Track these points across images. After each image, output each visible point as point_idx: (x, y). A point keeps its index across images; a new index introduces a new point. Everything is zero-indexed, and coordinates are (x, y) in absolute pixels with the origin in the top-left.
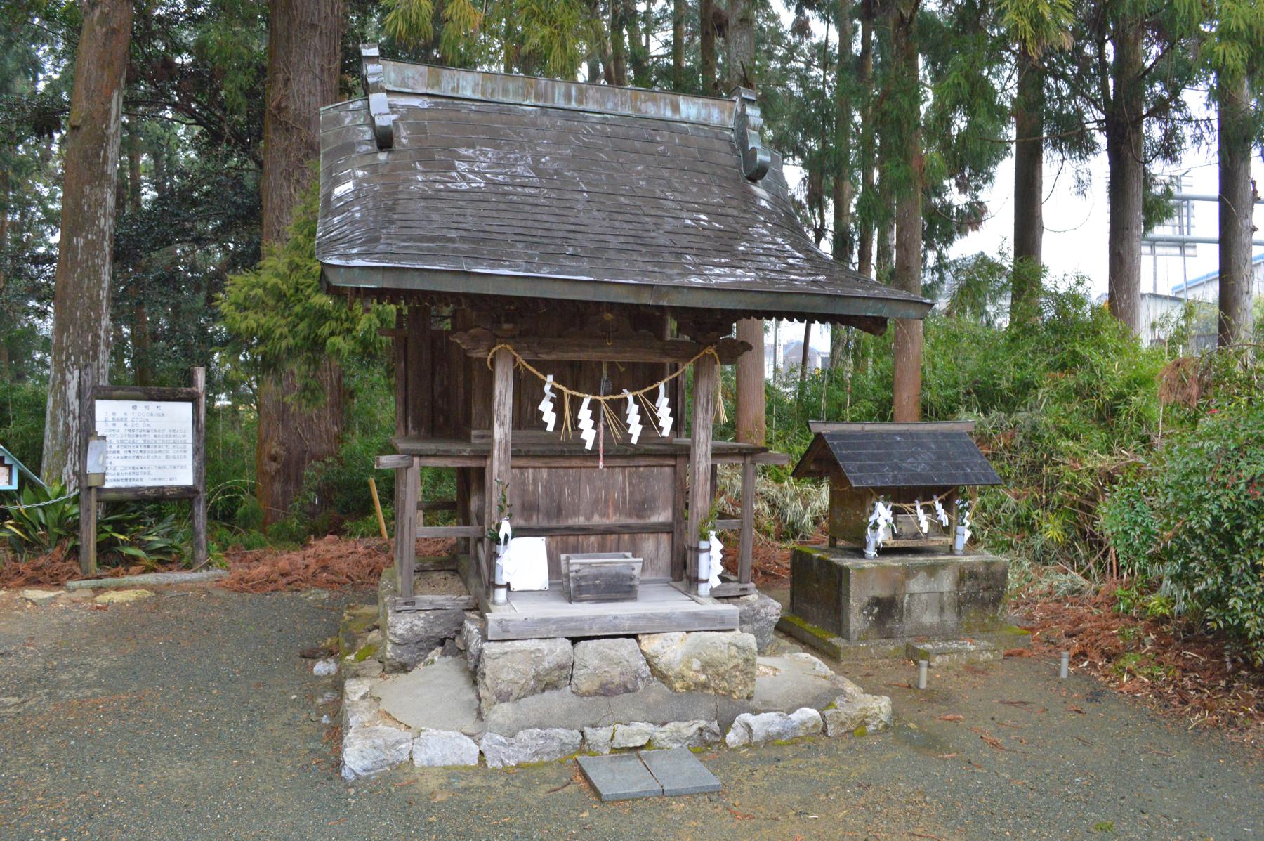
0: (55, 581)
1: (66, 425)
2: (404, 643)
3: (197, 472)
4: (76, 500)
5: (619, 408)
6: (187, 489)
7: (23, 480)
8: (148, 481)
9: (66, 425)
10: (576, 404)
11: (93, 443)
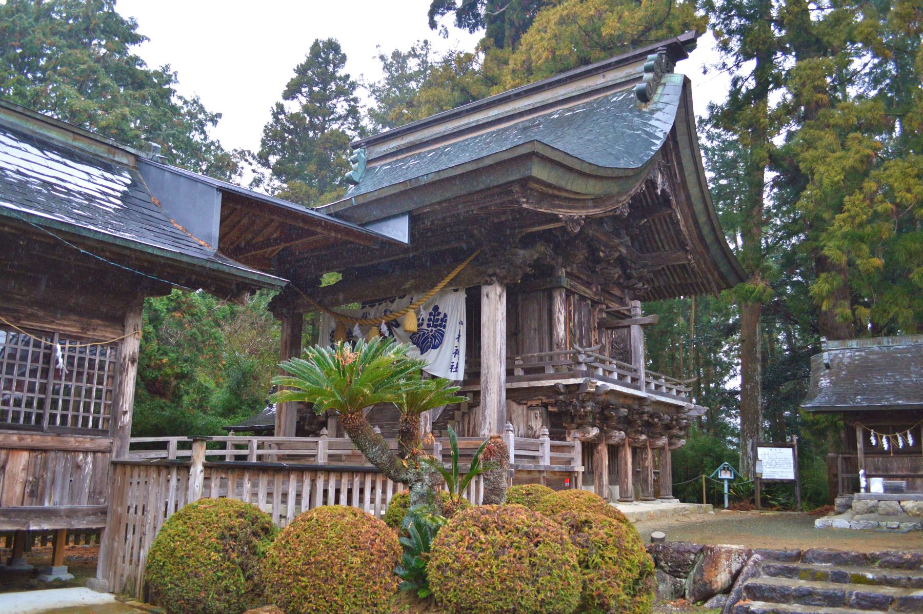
0: (747, 510)
2: (839, 506)
3: (795, 474)
4: (753, 483)
5: (896, 438)
6: (790, 482)
7: (735, 476)
8: (777, 477)
10: (882, 438)
11: (757, 462)
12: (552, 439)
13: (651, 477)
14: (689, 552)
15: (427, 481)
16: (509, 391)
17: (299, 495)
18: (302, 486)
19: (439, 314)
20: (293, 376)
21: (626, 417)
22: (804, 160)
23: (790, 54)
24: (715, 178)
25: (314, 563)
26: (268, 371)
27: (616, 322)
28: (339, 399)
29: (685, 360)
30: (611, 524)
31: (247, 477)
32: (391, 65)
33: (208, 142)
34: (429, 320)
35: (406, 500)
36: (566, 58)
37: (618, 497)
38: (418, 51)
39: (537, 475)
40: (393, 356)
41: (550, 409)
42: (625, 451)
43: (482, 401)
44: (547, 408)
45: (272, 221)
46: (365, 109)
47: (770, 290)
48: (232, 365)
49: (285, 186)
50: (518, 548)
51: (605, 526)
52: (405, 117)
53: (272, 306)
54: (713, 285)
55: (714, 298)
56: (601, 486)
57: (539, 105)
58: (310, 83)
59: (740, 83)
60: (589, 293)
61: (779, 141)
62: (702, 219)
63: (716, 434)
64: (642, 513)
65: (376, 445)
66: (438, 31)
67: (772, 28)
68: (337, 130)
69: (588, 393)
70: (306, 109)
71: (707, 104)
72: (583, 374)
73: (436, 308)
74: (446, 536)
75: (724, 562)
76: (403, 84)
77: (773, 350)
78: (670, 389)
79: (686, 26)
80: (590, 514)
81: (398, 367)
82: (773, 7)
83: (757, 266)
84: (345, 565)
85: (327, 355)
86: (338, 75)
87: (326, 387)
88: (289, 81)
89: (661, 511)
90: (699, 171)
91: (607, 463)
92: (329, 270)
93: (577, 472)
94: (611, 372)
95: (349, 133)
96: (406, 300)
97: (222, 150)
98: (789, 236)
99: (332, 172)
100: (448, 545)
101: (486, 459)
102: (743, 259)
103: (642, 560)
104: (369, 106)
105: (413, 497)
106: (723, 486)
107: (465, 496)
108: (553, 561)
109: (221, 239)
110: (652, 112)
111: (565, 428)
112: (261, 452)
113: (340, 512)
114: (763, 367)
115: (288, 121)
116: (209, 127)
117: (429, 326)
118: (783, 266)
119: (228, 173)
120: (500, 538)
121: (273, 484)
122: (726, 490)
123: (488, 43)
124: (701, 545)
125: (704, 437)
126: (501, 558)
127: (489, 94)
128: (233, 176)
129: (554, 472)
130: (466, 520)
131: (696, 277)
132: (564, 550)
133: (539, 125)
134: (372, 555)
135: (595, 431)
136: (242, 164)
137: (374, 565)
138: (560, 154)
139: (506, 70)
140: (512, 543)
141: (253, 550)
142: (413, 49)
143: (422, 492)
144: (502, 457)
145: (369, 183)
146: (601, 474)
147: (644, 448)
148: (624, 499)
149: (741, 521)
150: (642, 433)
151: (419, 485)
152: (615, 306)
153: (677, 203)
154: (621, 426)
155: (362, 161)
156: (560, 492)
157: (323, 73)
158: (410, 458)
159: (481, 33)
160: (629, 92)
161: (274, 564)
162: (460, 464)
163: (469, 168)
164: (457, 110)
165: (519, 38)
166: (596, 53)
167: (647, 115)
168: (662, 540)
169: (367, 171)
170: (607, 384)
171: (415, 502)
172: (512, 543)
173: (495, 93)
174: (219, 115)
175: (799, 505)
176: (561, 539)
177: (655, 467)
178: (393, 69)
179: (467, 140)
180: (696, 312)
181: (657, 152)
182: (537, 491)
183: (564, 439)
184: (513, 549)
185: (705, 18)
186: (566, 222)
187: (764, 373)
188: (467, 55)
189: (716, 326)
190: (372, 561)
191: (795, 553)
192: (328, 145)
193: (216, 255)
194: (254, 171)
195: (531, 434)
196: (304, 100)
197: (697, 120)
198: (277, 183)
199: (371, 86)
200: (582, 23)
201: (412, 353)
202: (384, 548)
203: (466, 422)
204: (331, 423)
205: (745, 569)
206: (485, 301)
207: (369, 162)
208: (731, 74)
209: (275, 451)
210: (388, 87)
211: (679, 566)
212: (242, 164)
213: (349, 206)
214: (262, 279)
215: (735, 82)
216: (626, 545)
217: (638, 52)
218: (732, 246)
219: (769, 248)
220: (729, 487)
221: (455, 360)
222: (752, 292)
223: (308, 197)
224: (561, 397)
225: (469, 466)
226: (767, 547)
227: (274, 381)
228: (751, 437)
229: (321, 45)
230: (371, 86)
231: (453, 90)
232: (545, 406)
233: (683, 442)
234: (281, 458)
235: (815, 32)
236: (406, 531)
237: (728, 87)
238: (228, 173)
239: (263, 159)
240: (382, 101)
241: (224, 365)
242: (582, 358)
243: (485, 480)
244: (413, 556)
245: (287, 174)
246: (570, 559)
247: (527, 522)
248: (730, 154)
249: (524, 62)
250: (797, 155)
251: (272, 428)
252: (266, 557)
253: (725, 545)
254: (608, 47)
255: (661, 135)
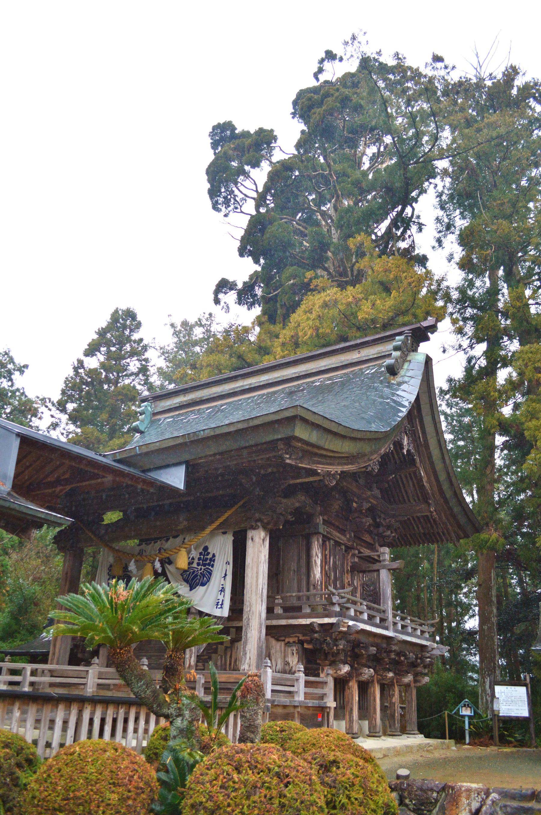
0: (487, 746)
1: (486, 699)
4: (491, 719)
6: (525, 719)
7: (475, 712)
8: (513, 714)
9: (486, 699)
11: (495, 700)
12: (306, 675)
13: (398, 712)
14: (432, 790)
15: (187, 716)
16: (268, 628)
17: (65, 723)
18: (69, 714)
19: (208, 553)
20: (69, 610)
21: (375, 655)
22: (529, 429)
23: (515, 339)
24: (454, 440)
25: (73, 798)
26: (48, 598)
27: (366, 566)
28: (110, 634)
29: (430, 600)
30: (357, 765)
31: (17, 705)
32: (180, 332)
33: (14, 388)
34: (199, 559)
35: (167, 733)
36: (327, 335)
37: (367, 733)
38: (204, 322)
39: (291, 710)
40: (162, 596)
41: (306, 646)
42: (374, 687)
43: (243, 637)
44: (303, 645)
45: (63, 464)
46: (155, 368)
47: (502, 540)
48: (14, 591)
49: (79, 430)
50: (269, 788)
51: (351, 766)
52: (189, 377)
53: (57, 539)
54: (453, 534)
55: (453, 547)
56: (351, 721)
57: (303, 373)
58: (108, 344)
59: (474, 361)
60: (343, 539)
61: (507, 411)
62: (442, 477)
63: (458, 671)
64: (389, 749)
65: (141, 679)
66: (221, 307)
67: (500, 317)
68: (129, 385)
69: (341, 632)
70: (103, 365)
71: (446, 377)
72: (336, 615)
73: (206, 549)
74: (202, 775)
75: (464, 801)
76: (189, 348)
77: (506, 592)
78: (415, 629)
79: (428, 314)
80: (338, 754)
81: (166, 606)
82: (499, 300)
83: (491, 518)
84: (102, 801)
85: (102, 591)
86: (133, 338)
87: (99, 623)
88: (91, 341)
89: (407, 747)
90: (439, 433)
91: (357, 698)
92: (112, 509)
93: (330, 708)
94: (361, 613)
95: (139, 387)
96: (179, 540)
97: (26, 396)
98: (518, 493)
99: (121, 420)
100: (203, 784)
101: (243, 696)
102: (479, 512)
103: (386, 801)
104: (159, 366)
105: (173, 732)
106: (464, 722)
107: (223, 730)
108: (302, 802)
109: (16, 476)
110: (400, 384)
111: (319, 664)
112: (33, 679)
113: (102, 746)
114: (498, 609)
115: (86, 375)
116: (16, 376)
117: (198, 564)
118: (515, 519)
119: (29, 417)
120: (252, 778)
121: (42, 711)
122: (467, 727)
123: (263, 320)
124: (443, 783)
125: (446, 674)
126: (252, 798)
127: (261, 362)
128: (33, 419)
129: (308, 708)
130: (220, 758)
131: (437, 528)
132: (313, 791)
133: (303, 390)
134: (129, 791)
135: (346, 669)
136: (42, 409)
137: (130, 802)
138: (320, 417)
139: (277, 342)
140: (264, 783)
141: (16, 782)
142: (200, 320)
143: (182, 727)
144: (259, 695)
145: (153, 432)
146: (352, 709)
147: (391, 685)
148: (372, 734)
149: (480, 758)
150: (389, 670)
151: (179, 720)
152: (367, 552)
153: (421, 461)
154: (370, 664)
155: (148, 414)
156: (311, 730)
157: (119, 336)
158: (172, 693)
159: (257, 310)
160: (380, 366)
161: (34, 797)
162: (220, 697)
163: (240, 426)
164: (234, 373)
165: (289, 316)
166: (352, 333)
167: (395, 387)
168: (407, 777)
169: (152, 422)
170: (358, 624)
171: (175, 737)
172: (264, 783)
173: (268, 361)
174: (26, 366)
175: (534, 742)
176: (310, 779)
177: (402, 702)
178: (182, 335)
179: (240, 400)
180: (439, 556)
181: (403, 419)
182: (290, 728)
183: (318, 675)
184: (264, 789)
185: (445, 307)
186: (323, 476)
187: (499, 615)
188: (244, 327)
189: (456, 571)
190: (129, 798)
191: (529, 792)
192: (120, 397)
193: (9, 494)
194: (52, 416)
195: (288, 670)
196: (102, 358)
197: (437, 391)
198: (72, 427)
199: (161, 348)
200: (342, 307)
201: (183, 589)
202: (141, 785)
203: (228, 656)
204: (103, 652)
205: (484, 808)
206: (249, 543)
207: (154, 414)
208: (466, 353)
209: (47, 679)
210: (175, 350)
211: (422, 804)
212: (42, 409)
213: (133, 454)
214: (48, 518)
215: (469, 360)
216: (372, 785)
217: (388, 334)
218: (468, 499)
219: (501, 503)
220: (470, 724)
221: (221, 597)
222: (487, 542)
223: (99, 441)
224: (316, 635)
225: (228, 699)
226: (504, 786)
227: (52, 614)
228: (489, 675)
229: (120, 312)
230: (161, 348)
231: (231, 356)
232: (301, 642)
233: (427, 679)
234: (52, 685)
235: (534, 323)
236: (164, 765)
237: (464, 363)
238: (29, 417)
239: (61, 406)
240: (170, 361)
241: (7, 591)
242: (335, 599)
243: (242, 716)
244: (170, 791)
245: (82, 420)
246: (318, 800)
247: (278, 762)
248: (467, 420)
249: (292, 336)
250: (523, 424)
251: (47, 654)
252: (26, 789)
253: (465, 784)
254: (362, 329)
255: (406, 404)
